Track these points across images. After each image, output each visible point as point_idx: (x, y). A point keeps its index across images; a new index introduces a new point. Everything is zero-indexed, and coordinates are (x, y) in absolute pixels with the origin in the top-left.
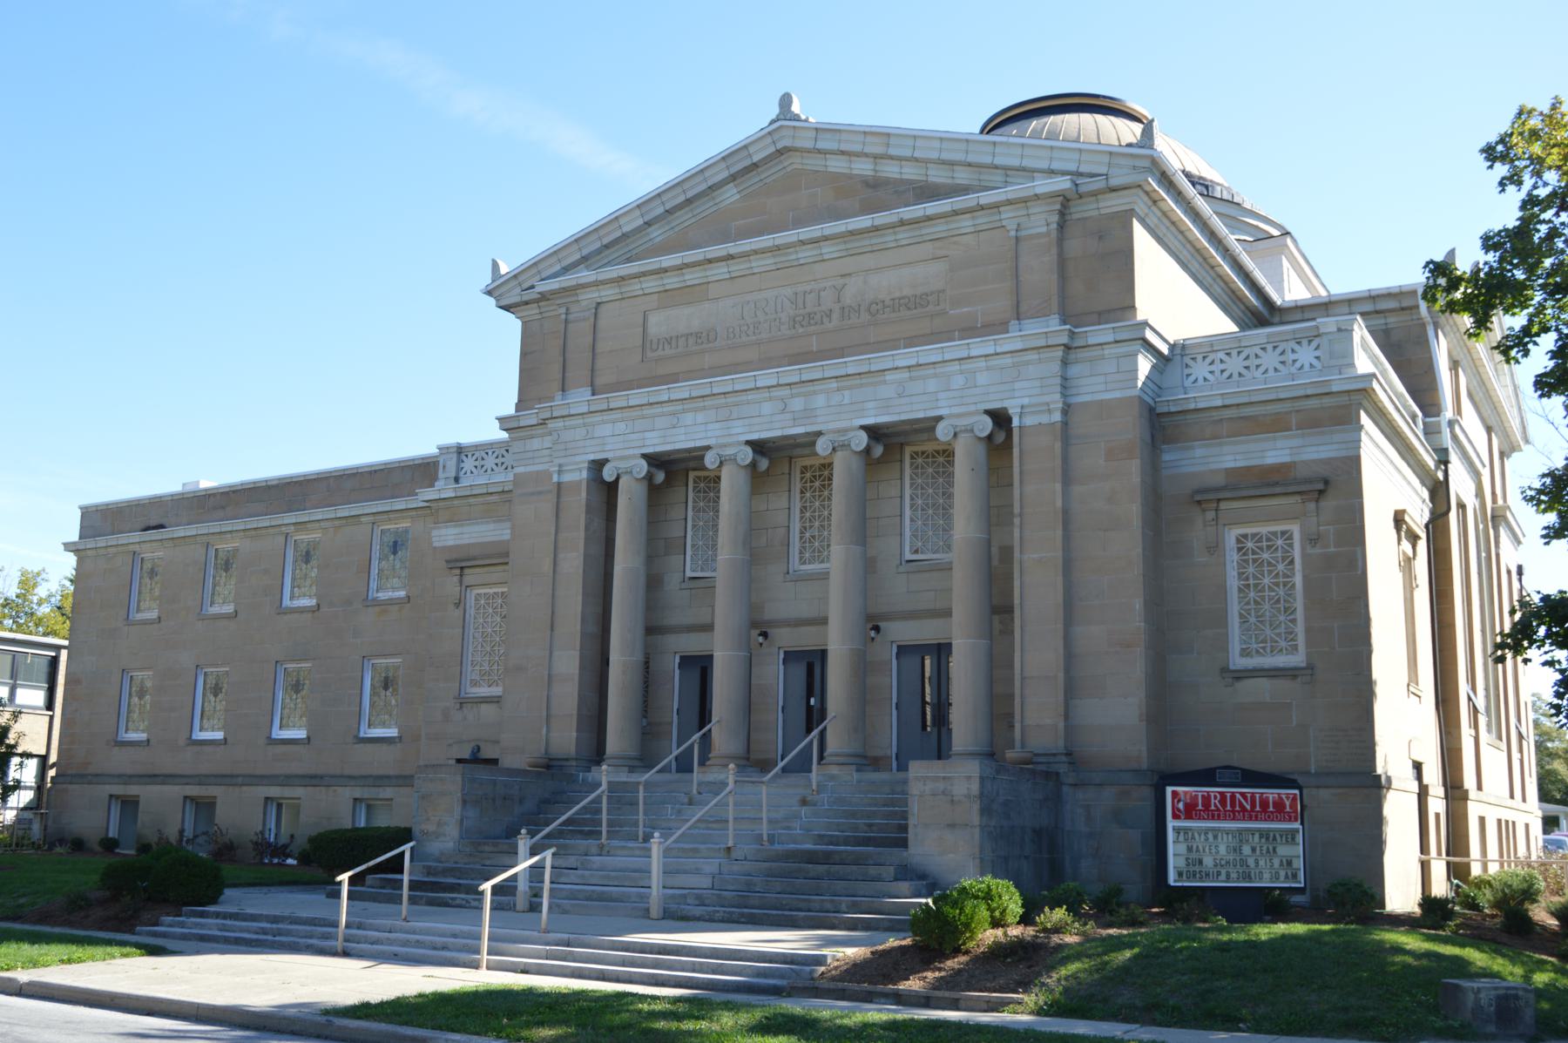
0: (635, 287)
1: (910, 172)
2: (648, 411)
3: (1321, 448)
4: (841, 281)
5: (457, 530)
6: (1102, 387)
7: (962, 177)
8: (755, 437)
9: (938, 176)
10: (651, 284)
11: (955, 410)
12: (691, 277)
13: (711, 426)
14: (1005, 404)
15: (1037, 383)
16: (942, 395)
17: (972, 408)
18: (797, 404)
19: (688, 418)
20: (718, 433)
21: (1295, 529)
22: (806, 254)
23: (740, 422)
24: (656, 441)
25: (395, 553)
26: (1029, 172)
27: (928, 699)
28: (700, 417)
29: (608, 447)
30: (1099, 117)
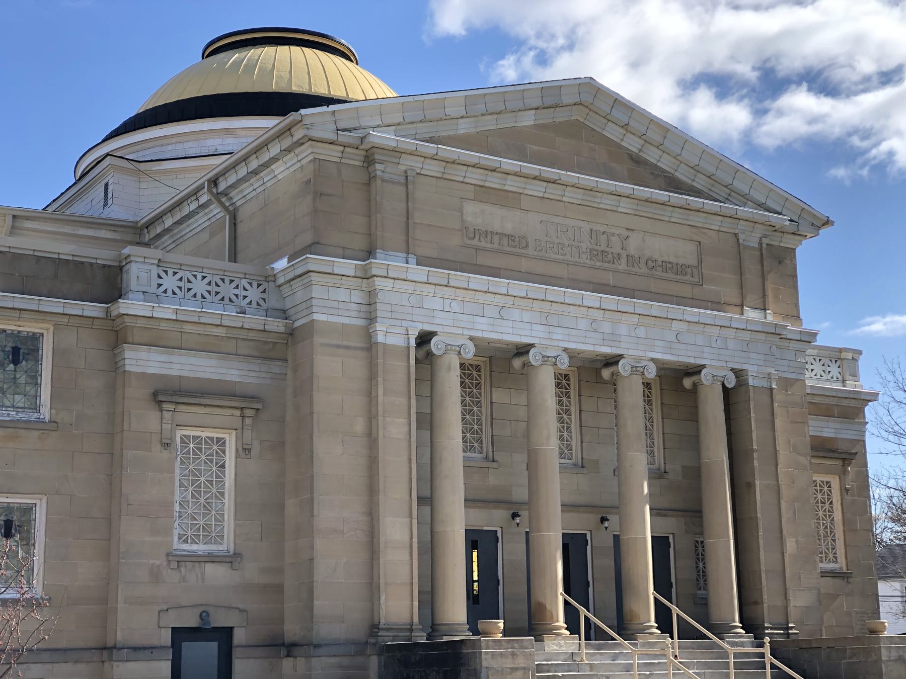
0: (458, 173)
1: (666, 163)
2: (480, 297)
3: (850, 432)
4: (626, 233)
5: (163, 358)
6: (786, 369)
7: (700, 183)
8: (572, 346)
9: (683, 174)
10: (475, 176)
11: (714, 363)
12: (512, 184)
13: (535, 327)
14: (744, 367)
15: (762, 357)
16: (706, 349)
17: (724, 364)
18: (606, 327)
19: (516, 314)
20: (541, 335)
21: (231, 441)
22: (608, 202)
23: (560, 330)
24: (485, 327)
25: (16, 362)
26: (745, 199)
27: (475, 578)
28: (527, 316)
29: (437, 321)
30: (296, 50)
